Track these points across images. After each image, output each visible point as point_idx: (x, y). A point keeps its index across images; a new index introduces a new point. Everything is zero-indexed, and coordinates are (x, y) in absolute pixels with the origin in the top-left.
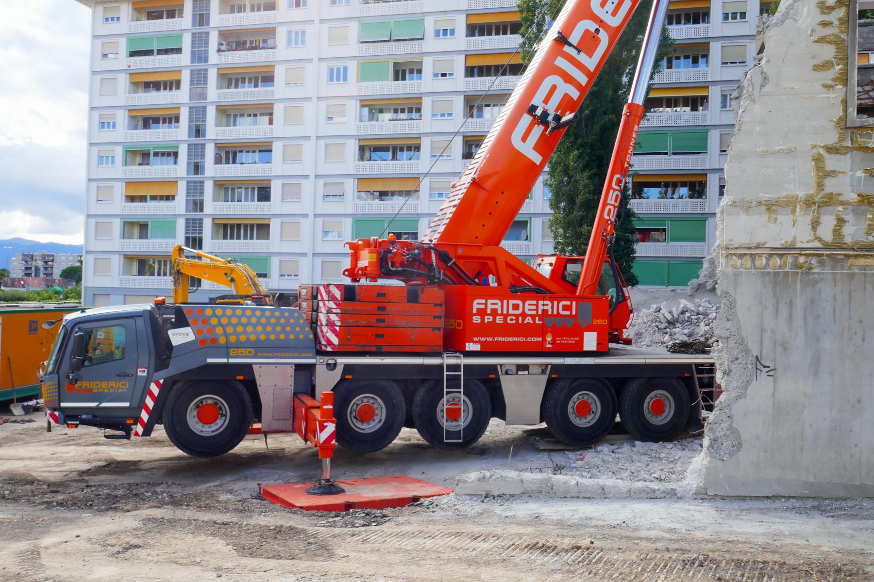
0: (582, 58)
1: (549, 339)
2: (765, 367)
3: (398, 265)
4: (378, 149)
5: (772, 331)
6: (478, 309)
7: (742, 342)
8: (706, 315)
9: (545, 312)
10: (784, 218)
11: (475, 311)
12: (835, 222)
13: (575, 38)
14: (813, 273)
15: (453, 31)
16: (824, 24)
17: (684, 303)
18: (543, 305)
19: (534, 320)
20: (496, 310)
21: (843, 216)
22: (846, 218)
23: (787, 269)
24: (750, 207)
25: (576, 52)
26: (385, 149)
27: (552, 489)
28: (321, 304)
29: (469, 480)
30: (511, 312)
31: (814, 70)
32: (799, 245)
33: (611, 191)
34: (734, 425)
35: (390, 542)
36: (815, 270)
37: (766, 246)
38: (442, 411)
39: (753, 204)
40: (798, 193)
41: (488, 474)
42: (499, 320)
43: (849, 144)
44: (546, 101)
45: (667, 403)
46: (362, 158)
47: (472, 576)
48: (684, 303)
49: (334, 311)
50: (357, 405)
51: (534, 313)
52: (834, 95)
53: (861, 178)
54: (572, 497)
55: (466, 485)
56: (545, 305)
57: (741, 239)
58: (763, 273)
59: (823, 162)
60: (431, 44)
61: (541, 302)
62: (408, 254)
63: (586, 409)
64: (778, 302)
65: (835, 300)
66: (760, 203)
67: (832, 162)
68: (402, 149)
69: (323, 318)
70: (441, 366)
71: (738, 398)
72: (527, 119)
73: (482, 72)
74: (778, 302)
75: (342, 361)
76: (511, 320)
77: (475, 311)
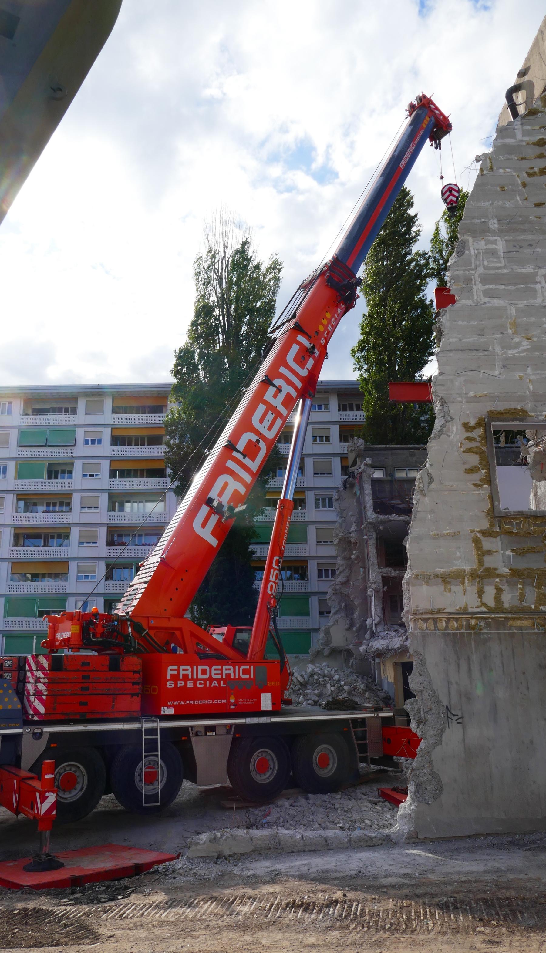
0: (247, 461)
1: (232, 701)
2: (454, 715)
3: (98, 635)
4: (30, 537)
5: (457, 684)
6: (171, 675)
7: (434, 695)
8: (331, 677)
9: (228, 675)
10: (457, 588)
11: (169, 677)
12: (495, 591)
13: (241, 445)
14: (483, 633)
15: (100, 441)
16: (469, 439)
17: (310, 668)
18: (227, 670)
19: (219, 683)
20: (187, 675)
21: (500, 586)
22: (503, 587)
23: (463, 630)
24: (429, 579)
25: (242, 457)
26: (37, 537)
27: (280, 844)
28: (29, 674)
29: (201, 842)
30: (200, 676)
31: (465, 472)
32: (470, 610)
33: (272, 570)
34: (435, 770)
35: (148, 915)
36: (485, 631)
37: (445, 611)
38: (140, 775)
39: (432, 577)
40: (464, 568)
41: (219, 834)
42: (190, 684)
43: (498, 530)
44: (220, 495)
45: (330, 756)
46: (16, 544)
47: (253, 943)
48: (310, 668)
49: (42, 680)
50: (60, 774)
51: (219, 677)
52: (483, 492)
53: (509, 556)
54: (299, 851)
55: (199, 847)
56: (229, 670)
57: (424, 605)
58: (444, 635)
59: (481, 543)
60: (81, 450)
61: (225, 667)
62: (108, 626)
63: (265, 766)
64: (458, 659)
65: (502, 655)
66: (436, 576)
67: (487, 544)
68: (52, 537)
69: (30, 688)
70: (138, 732)
71: (435, 745)
72: (205, 510)
73: (124, 474)
74: (458, 659)
75: (48, 729)
76: (200, 684)
77: (169, 677)
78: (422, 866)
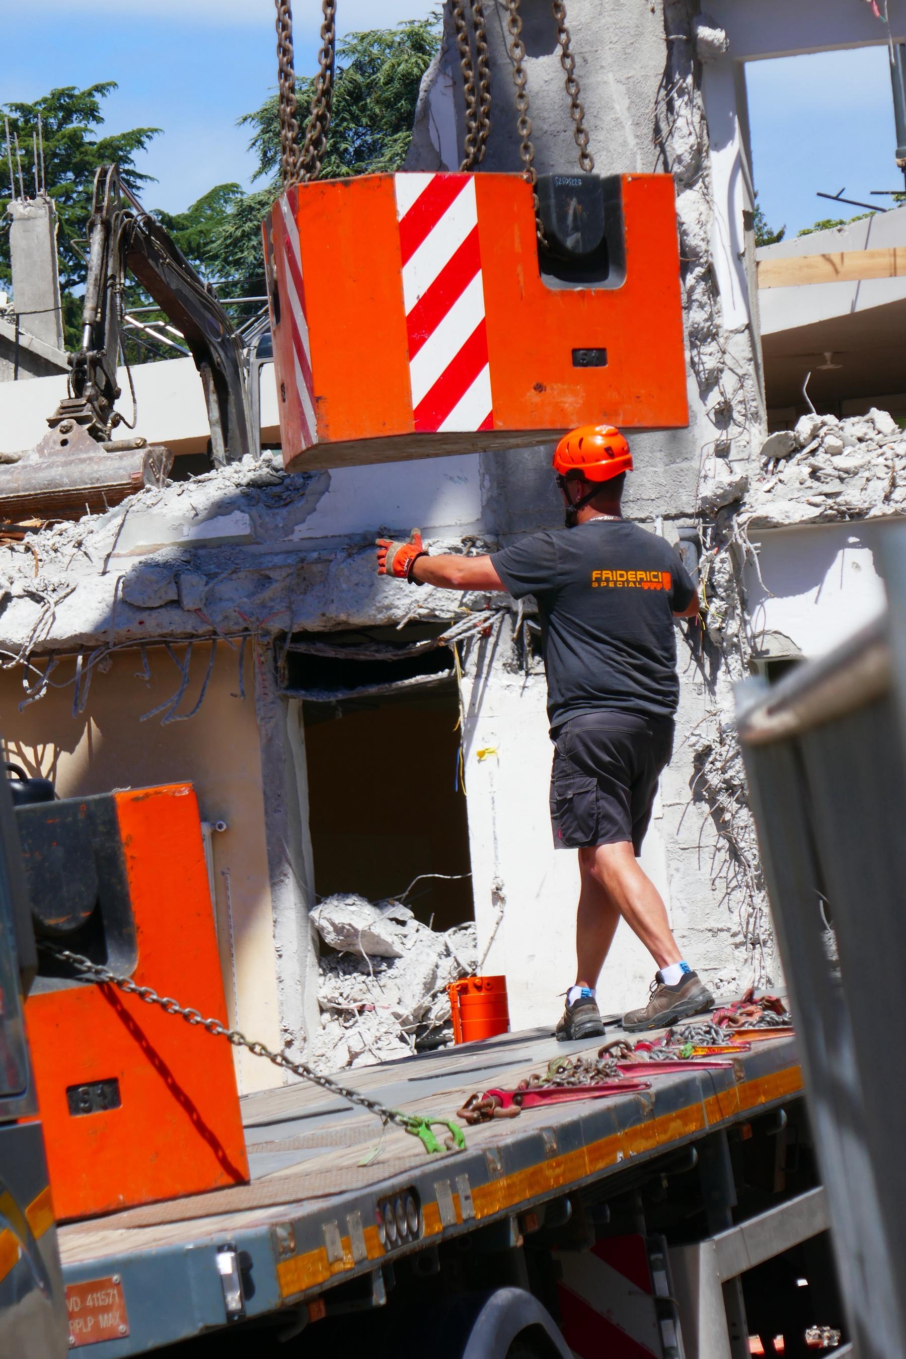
30: (619, 579)
42: (611, 585)
78: (77, 291)
